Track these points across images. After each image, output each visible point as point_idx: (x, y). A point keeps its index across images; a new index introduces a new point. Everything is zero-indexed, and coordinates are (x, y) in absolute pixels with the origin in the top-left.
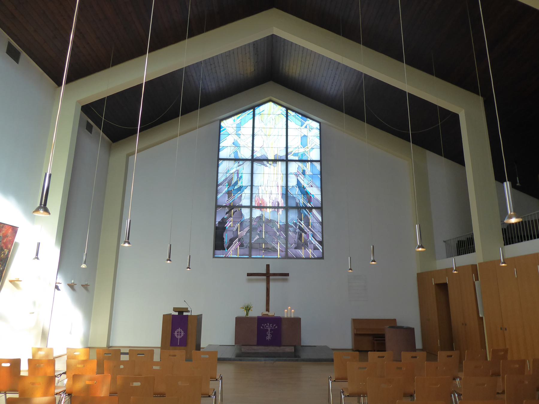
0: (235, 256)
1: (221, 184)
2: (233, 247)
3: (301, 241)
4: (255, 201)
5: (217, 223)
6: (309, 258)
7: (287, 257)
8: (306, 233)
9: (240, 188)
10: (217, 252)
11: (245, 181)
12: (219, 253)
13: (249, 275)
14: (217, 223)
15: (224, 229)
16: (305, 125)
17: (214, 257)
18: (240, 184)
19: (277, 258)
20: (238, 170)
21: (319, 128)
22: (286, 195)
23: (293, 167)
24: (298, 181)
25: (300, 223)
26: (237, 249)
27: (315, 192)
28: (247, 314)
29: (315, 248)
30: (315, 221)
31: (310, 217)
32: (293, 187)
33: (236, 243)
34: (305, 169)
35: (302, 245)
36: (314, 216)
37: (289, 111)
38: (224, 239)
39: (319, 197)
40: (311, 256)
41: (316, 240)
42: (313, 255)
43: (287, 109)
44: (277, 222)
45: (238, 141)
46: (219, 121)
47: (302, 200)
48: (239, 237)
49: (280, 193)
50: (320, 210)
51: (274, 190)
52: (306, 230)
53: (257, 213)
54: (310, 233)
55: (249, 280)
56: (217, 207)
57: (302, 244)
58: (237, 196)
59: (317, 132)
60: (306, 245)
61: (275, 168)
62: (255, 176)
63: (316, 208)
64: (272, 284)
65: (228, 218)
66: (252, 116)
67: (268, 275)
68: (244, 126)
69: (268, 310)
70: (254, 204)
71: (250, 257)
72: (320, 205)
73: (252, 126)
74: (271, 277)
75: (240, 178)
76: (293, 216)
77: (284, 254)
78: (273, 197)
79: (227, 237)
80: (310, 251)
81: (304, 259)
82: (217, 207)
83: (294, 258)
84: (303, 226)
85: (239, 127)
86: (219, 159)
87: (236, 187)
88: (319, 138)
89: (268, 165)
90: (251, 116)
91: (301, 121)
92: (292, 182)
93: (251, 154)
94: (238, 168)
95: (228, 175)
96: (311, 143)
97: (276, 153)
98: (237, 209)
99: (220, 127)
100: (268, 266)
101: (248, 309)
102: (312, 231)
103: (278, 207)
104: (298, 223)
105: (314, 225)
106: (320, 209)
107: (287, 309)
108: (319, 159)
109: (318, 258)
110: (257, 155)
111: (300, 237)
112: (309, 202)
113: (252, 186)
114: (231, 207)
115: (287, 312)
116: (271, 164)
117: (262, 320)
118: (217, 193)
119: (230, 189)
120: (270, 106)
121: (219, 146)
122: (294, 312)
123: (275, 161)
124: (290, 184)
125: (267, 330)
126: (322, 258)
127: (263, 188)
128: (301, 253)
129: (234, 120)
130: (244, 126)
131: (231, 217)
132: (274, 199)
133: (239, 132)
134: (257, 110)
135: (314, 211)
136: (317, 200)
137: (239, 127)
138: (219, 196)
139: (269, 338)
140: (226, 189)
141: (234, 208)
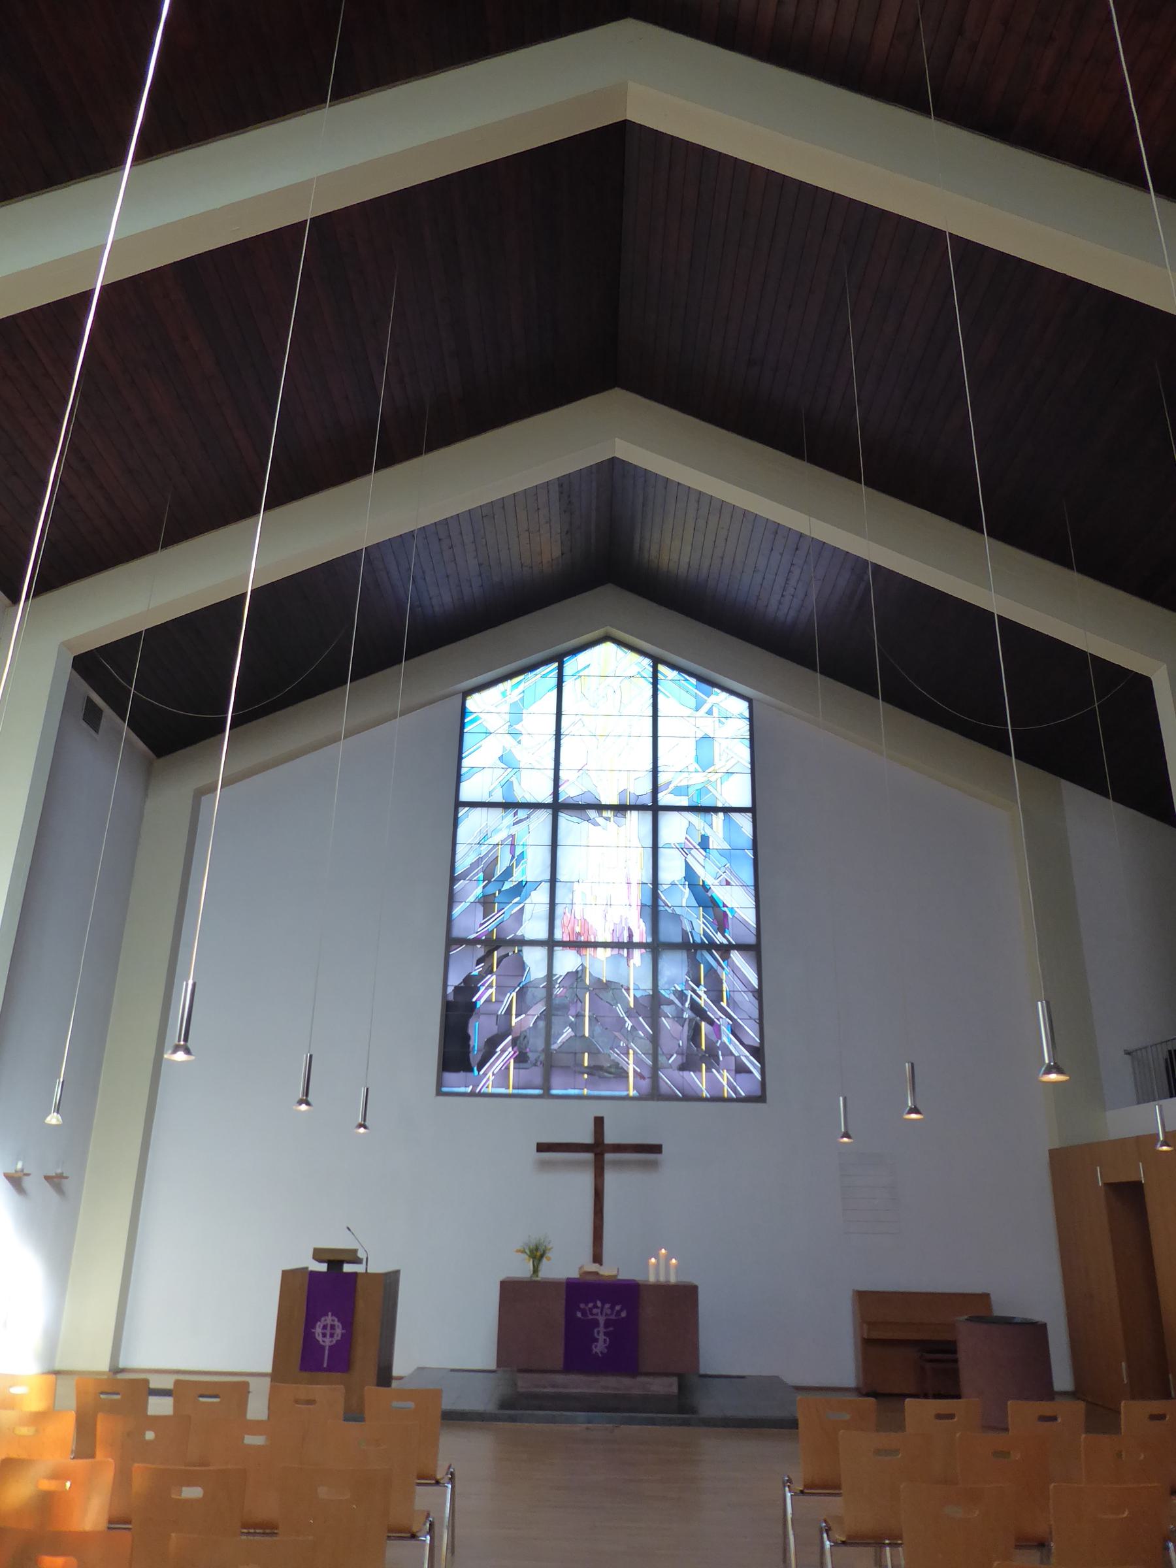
0: (502, 1091)
1: (464, 876)
3: (698, 1045)
4: (563, 926)
5: (450, 990)
6: (721, 1099)
8: (711, 1022)
9: (520, 889)
10: (449, 1077)
12: (456, 1082)
13: (542, 1148)
14: (450, 990)
16: (705, 708)
17: (439, 1093)
18: (517, 876)
19: (627, 1098)
22: (654, 909)
23: (674, 827)
25: (694, 991)
26: (508, 1068)
27: (739, 901)
28: (536, 1271)
29: (741, 1069)
30: (739, 986)
32: (673, 884)
33: (505, 1055)
36: (735, 970)
37: (662, 668)
39: (750, 917)
40: (727, 1092)
42: (735, 1091)
43: (656, 661)
44: (628, 990)
47: (699, 925)
50: (753, 953)
52: (714, 1012)
53: (566, 961)
54: (724, 1023)
55: (543, 1165)
56: (452, 942)
58: (511, 909)
59: (744, 727)
60: (711, 1057)
63: (741, 947)
64: (610, 1177)
65: (481, 977)
66: (555, 681)
67: (599, 1150)
69: (597, 1258)
70: (558, 935)
72: (752, 940)
74: (608, 1157)
76: (674, 970)
77: (646, 1084)
78: (615, 915)
79: (478, 1031)
80: (724, 1077)
81: (706, 1100)
82: (452, 942)
84: (704, 1000)
85: (516, 713)
86: (459, 804)
88: (747, 743)
89: (600, 820)
91: (696, 696)
92: (672, 870)
93: (551, 790)
95: (484, 849)
99: (463, 712)
100: (599, 1122)
101: (537, 1254)
103: (630, 945)
104: (689, 993)
106: (753, 950)
108: (747, 802)
109: (748, 1099)
110: (569, 792)
113: (553, 881)
114: (492, 944)
116: (608, 819)
117: (580, 1291)
118: (452, 901)
121: (459, 767)
122: (677, 1267)
123: (621, 809)
124: (665, 877)
125: (596, 1323)
126: (761, 1098)
128: (700, 1081)
131: (491, 972)
133: (518, 727)
134: (572, 665)
135: (735, 956)
136: (745, 924)
137: (516, 713)
138: (457, 910)
140: (478, 891)
141: (500, 947)
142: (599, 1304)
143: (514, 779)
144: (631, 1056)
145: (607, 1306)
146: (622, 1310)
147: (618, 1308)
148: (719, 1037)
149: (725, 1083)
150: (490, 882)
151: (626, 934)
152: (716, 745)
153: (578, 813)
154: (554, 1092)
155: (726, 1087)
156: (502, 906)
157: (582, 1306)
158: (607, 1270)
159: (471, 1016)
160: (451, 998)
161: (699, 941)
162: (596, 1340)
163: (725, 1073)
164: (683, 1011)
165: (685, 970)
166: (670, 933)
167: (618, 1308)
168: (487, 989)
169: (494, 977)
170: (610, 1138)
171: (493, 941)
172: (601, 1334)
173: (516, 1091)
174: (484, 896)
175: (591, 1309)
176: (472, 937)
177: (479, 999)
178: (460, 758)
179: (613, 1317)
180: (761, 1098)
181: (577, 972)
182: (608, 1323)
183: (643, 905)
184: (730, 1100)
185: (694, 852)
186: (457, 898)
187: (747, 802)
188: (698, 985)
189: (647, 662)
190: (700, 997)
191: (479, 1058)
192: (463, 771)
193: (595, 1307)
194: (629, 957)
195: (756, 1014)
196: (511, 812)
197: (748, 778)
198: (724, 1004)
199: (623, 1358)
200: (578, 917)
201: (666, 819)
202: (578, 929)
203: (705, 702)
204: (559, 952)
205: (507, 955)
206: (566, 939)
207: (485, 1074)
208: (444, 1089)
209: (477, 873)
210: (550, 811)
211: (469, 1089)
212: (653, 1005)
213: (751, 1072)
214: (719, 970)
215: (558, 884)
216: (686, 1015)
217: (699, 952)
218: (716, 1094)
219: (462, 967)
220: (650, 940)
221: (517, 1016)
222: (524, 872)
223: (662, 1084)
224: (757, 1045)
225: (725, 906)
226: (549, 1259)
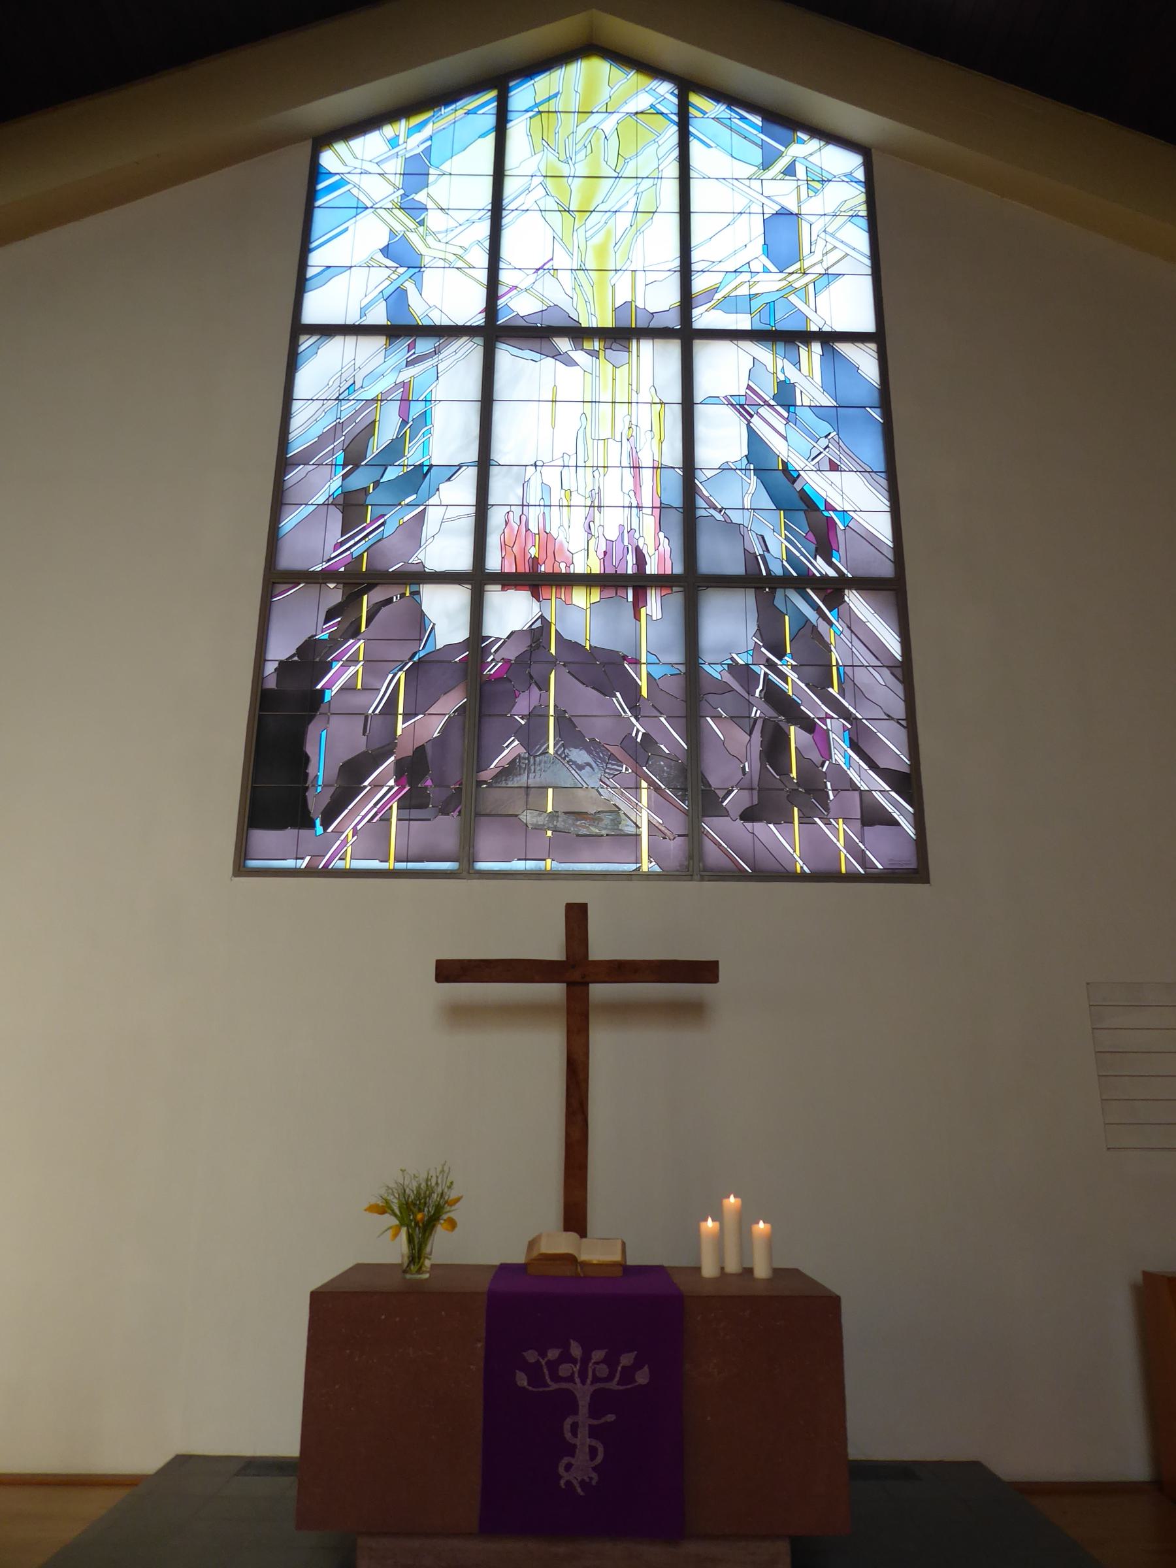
0: (375, 864)
1: (305, 458)
2: (360, 813)
3: (784, 771)
4: (504, 545)
5: (270, 668)
6: (832, 876)
7: (694, 866)
8: (809, 726)
9: (419, 476)
10: (263, 838)
11: (449, 437)
12: (276, 847)
13: (448, 971)
14: (270, 668)
15: (313, 702)
16: (782, 164)
17: (240, 870)
18: (413, 456)
19: (636, 875)
20: (406, 385)
21: (860, 174)
22: (687, 512)
23: (723, 369)
24: (753, 437)
26: (386, 819)
27: (858, 500)
28: (417, 1254)
29: (873, 816)
30: (863, 656)
31: (835, 634)
32: (724, 468)
33: (382, 787)
34: (792, 374)
35: (792, 797)
36: (853, 625)
37: (695, 99)
38: (306, 760)
39: (881, 526)
40: (846, 862)
41: (873, 766)
42: (862, 859)
43: (686, 86)
44: (636, 662)
45: (414, 238)
46: (307, 146)
47: (778, 545)
48: (405, 749)
49: (647, 501)
50: (888, 595)
51: (615, 487)
52: (813, 706)
53: (510, 613)
54: (835, 727)
55: (459, 1014)
56: (277, 577)
57: (792, 790)
58: (396, 519)
59: (856, 196)
60: (811, 793)
61: (622, 372)
62: (500, 412)
63: (864, 584)
64: (603, 1042)
65: (334, 642)
66: (490, 121)
67: (576, 976)
68: (446, 167)
69: (575, 1218)
70: (494, 562)
71: (467, 871)
72: (886, 569)
73: (489, 168)
74: (599, 991)
75: (414, 423)
76: (729, 628)
77: (675, 847)
78: (611, 523)
79: (326, 749)
80: (840, 834)
81: (802, 877)
82: (277, 577)
83: (739, 875)
84: (793, 683)
85: (417, 173)
86: (299, 329)
87: (391, 474)
88: (864, 223)
89: (579, 356)
90: (488, 120)
91: (763, 146)
92: (721, 441)
93: (482, 304)
94: (406, 375)
95: (347, 409)
96: (819, 248)
97: (622, 297)
98: (394, 592)
99: (315, 172)
100: (577, 915)
101: (420, 1213)
102: (847, 716)
103: (641, 583)
104: (762, 670)
105: (861, 677)
106: (891, 590)
107: (718, 1217)
108: (867, 324)
109: (891, 876)
110: (520, 306)
111: (774, 748)
112: (825, 548)
113: (484, 463)
114: (357, 581)
115: (720, 1238)
116: (594, 354)
117: (532, 1308)
118: (279, 502)
119: (359, 480)
120: (588, 76)
121: (303, 264)
122: (771, 1242)
123: (620, 335)
124: (708, 455)
125: (568, 1403)
126: (918, 873)
127: (551, 476)
128: (788, 842)
129: (393, 142)
130: (446, 167)
131: (355, 633)
132: (613, 535)
133: (421, 197)
134: (522, 96)
135: (855, 601)
136: (871, 540)
137: (417, 173)
138: (290, 521)
139: (579, 1468)
140: (336, 484)
141: (372, 587)
142: (576, 1351)
143: (410, 287)
144: (644, 793)
146: (637, 1365)
147: (627, 1360)
149: (841, 844)
150: (356, 466)
151: (631, 559)
152: (805, 227)
153: (536, 343)
154: (482, 866)
155: (844, 852)
156: (381, 510)
157: (531, 1356)
158: (596, 1251)
159: (310, 719)
160: (271, 684)
161: (777, 570)
162: (571, 1450)
163: (841, 825)
164: (750, 705)
165: (753, 628)
166: (719, 557)
167: (627, 1360)
168: (346, 665)
169: (361, 643)
170: (600, 949)
171: (360, 575)
172: (583, 1432)
173: (402, 866)
174: (346, 494)
175: (553, 1366)
176: (318, 568)
177: (329, 686)
178: (305, 249)
179: (613, 1385)
181: (531, 630)
182: (600, 1403)
183: (663, 507)
184: (852, 877)
185: (764, 411)
186: (290, 497)
187: (867, 324)
189: (665, 89)
190: (784, 677)
191: (326, 800)
192: (311, 272)
193: (566, 1357)
195: (899, 710)
196: (404, 343)
197: (867, 284)
198: (834, 691)
199: (645, 1492)
200: (533, 528)
201: (708, 355)
202: (533, 552)
203: (780, 154)
204: (495, 597)
205: (389, 601)
206: (510, 568)
207: (338, 832)
208: (252, 864)
209: (333, 452)
210: (480, 341)
211: (303, 864)
212: (693, 690)
213: (897, 824)
214: (822, 627)
215: (494, 471)
216: (755, 713)
217: (779, 593)
218: (823, 866)
219: (298, 623)
220: (678, 570)
221: (407, 716)
222: (426, 447)
223: (709, 846)
224: (906, 770)
225: (829, 507)
226: (452, 1224)
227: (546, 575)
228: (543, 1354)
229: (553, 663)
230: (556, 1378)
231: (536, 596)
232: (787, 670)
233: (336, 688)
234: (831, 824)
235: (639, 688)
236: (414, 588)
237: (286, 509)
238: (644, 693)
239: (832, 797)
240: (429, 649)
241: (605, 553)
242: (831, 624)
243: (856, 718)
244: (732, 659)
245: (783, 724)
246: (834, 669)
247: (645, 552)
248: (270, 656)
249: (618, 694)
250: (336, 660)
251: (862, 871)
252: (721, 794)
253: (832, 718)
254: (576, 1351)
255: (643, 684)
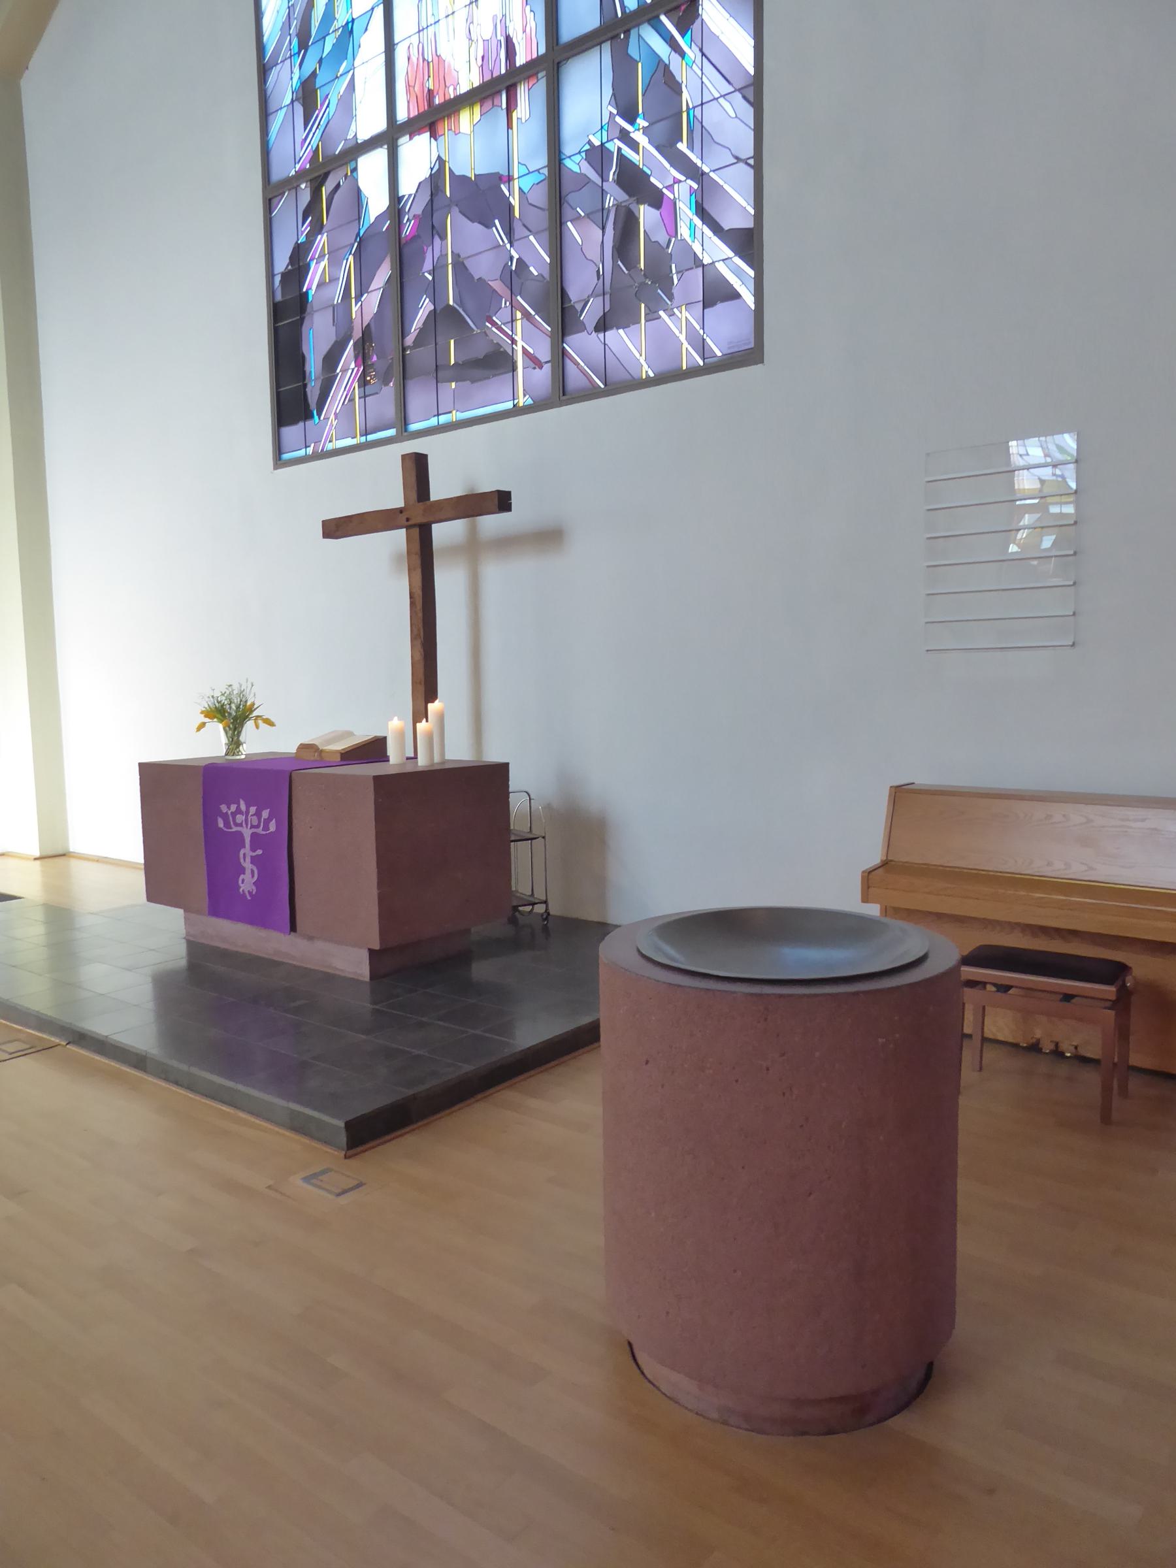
3: (631, 264)
8: (656, 199)
10: (291, 433)
14: (278, 279)
18: (341, 18)
19: (517, 411)
25: (624, 136)
26: (352, 400)
28: (235, 743)
29: (717, 293)
40: (690, 356)
41: (717, 229)
44: (510, 179)
52: (662, 174)
77: (543, 376)
84: (645, 153)
101: (233, 715)
102: (696, 174)
126: (749, 356)
128: (631, 346)
139: (247, 883)
142: (243, 807)
144: (519, 323)
145: (253, 810)
148: (672, 228)
154: (414, 427)
172: (248, 859)
175: (234, 814)
176: (293, 173)
177: (309, 288)
179: (260, 831)
180: (749, 356)
182: (256, 840)
188: (631, 119)
190: (634, 146)
194: (511, 106)
198: (682, 146)
202: (430, 84)
205: (338, 186)
207: (327, 419)
211: (310, 450)
216: (610, 202)
218: (665, 366)
227: (440, 105)
228: (229, 808)
229: (448, 208)
230: (236, 825)
231: (434, 135)
232: (638, 136)
233: (314, 287)
234: (674, 314)
235: (511, 207)
236: (353, 165)
237: (271, 118)
238: (517, 214)
239: (676, 281)
240: (366, 225)
241: (483, 57)
242: (682, 54)
243: (703, 173)
244: (590, 142)
245: (633, 207)
246: (685, 115)
247: (514, 41)
248: (276, 271)
249: (497, 222)
250: (312, 259)
251: (701, 363)
252: (579, 307)
253: (680, 181)
254: (243, 807)
255: (515, 202)
